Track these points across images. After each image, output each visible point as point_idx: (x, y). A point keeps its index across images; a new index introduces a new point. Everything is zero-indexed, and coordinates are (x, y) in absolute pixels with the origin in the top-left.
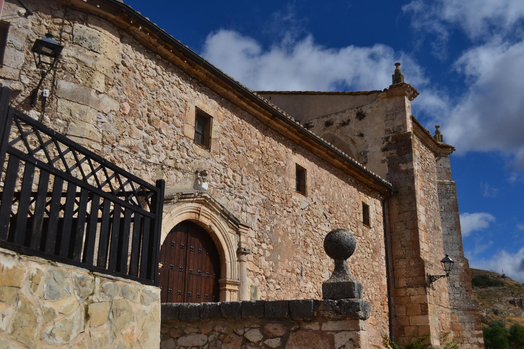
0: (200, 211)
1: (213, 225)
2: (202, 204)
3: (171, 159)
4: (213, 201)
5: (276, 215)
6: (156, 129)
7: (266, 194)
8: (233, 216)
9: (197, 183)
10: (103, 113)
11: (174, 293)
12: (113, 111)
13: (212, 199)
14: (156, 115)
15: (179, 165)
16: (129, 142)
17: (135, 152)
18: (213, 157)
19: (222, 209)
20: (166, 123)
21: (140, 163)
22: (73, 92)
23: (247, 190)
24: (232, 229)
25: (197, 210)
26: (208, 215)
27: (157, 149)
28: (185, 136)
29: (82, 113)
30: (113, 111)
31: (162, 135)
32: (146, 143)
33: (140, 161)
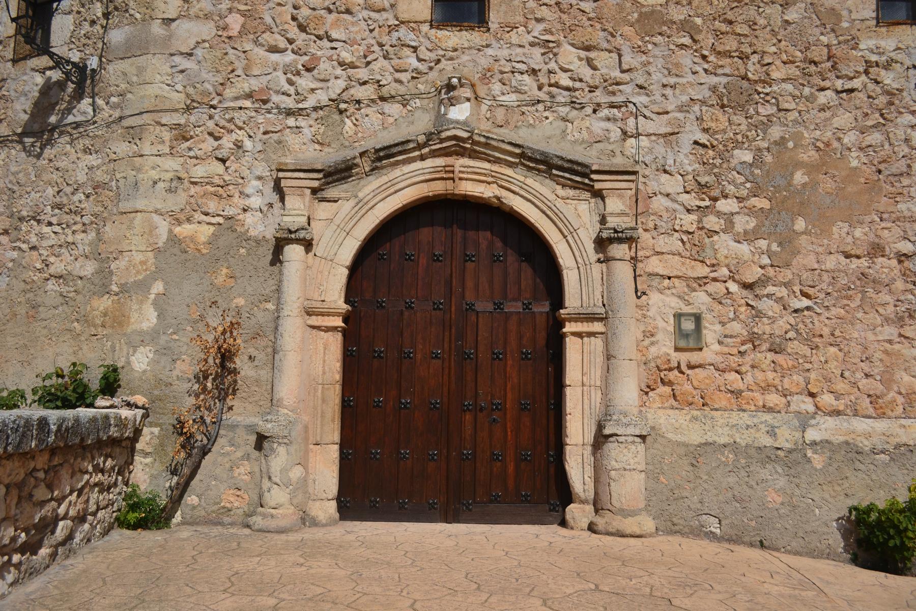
0: (453, 172)
1: (504, 193)
2: (457, 154)
3: (365, 83)
4: (483, 140)
5: (782, 114)
6: (320, 38)
7: (727, 70)
8: (562, 159)
9: (439, 110)
10: (182, 54)
11: (419, 356)
12: (204, 41)
13: (476, 138)
14: (314, 9)
15: (392, 89)
16: (245, 85)
17: (265, 102)
18: (498, 40)
19: (518, 151)
20: (346, 16)
21: (281, 117)
22: (128, 40)
23: (640, 81)
24: (575, 188)
25: (446, 172)
26: (485, 175)
27: (322, 77)
28: (402, 23)
29: (141, 70)
30: (204, 41)
31: (334, 44)
32: (292, 72)
33: (280, 113)
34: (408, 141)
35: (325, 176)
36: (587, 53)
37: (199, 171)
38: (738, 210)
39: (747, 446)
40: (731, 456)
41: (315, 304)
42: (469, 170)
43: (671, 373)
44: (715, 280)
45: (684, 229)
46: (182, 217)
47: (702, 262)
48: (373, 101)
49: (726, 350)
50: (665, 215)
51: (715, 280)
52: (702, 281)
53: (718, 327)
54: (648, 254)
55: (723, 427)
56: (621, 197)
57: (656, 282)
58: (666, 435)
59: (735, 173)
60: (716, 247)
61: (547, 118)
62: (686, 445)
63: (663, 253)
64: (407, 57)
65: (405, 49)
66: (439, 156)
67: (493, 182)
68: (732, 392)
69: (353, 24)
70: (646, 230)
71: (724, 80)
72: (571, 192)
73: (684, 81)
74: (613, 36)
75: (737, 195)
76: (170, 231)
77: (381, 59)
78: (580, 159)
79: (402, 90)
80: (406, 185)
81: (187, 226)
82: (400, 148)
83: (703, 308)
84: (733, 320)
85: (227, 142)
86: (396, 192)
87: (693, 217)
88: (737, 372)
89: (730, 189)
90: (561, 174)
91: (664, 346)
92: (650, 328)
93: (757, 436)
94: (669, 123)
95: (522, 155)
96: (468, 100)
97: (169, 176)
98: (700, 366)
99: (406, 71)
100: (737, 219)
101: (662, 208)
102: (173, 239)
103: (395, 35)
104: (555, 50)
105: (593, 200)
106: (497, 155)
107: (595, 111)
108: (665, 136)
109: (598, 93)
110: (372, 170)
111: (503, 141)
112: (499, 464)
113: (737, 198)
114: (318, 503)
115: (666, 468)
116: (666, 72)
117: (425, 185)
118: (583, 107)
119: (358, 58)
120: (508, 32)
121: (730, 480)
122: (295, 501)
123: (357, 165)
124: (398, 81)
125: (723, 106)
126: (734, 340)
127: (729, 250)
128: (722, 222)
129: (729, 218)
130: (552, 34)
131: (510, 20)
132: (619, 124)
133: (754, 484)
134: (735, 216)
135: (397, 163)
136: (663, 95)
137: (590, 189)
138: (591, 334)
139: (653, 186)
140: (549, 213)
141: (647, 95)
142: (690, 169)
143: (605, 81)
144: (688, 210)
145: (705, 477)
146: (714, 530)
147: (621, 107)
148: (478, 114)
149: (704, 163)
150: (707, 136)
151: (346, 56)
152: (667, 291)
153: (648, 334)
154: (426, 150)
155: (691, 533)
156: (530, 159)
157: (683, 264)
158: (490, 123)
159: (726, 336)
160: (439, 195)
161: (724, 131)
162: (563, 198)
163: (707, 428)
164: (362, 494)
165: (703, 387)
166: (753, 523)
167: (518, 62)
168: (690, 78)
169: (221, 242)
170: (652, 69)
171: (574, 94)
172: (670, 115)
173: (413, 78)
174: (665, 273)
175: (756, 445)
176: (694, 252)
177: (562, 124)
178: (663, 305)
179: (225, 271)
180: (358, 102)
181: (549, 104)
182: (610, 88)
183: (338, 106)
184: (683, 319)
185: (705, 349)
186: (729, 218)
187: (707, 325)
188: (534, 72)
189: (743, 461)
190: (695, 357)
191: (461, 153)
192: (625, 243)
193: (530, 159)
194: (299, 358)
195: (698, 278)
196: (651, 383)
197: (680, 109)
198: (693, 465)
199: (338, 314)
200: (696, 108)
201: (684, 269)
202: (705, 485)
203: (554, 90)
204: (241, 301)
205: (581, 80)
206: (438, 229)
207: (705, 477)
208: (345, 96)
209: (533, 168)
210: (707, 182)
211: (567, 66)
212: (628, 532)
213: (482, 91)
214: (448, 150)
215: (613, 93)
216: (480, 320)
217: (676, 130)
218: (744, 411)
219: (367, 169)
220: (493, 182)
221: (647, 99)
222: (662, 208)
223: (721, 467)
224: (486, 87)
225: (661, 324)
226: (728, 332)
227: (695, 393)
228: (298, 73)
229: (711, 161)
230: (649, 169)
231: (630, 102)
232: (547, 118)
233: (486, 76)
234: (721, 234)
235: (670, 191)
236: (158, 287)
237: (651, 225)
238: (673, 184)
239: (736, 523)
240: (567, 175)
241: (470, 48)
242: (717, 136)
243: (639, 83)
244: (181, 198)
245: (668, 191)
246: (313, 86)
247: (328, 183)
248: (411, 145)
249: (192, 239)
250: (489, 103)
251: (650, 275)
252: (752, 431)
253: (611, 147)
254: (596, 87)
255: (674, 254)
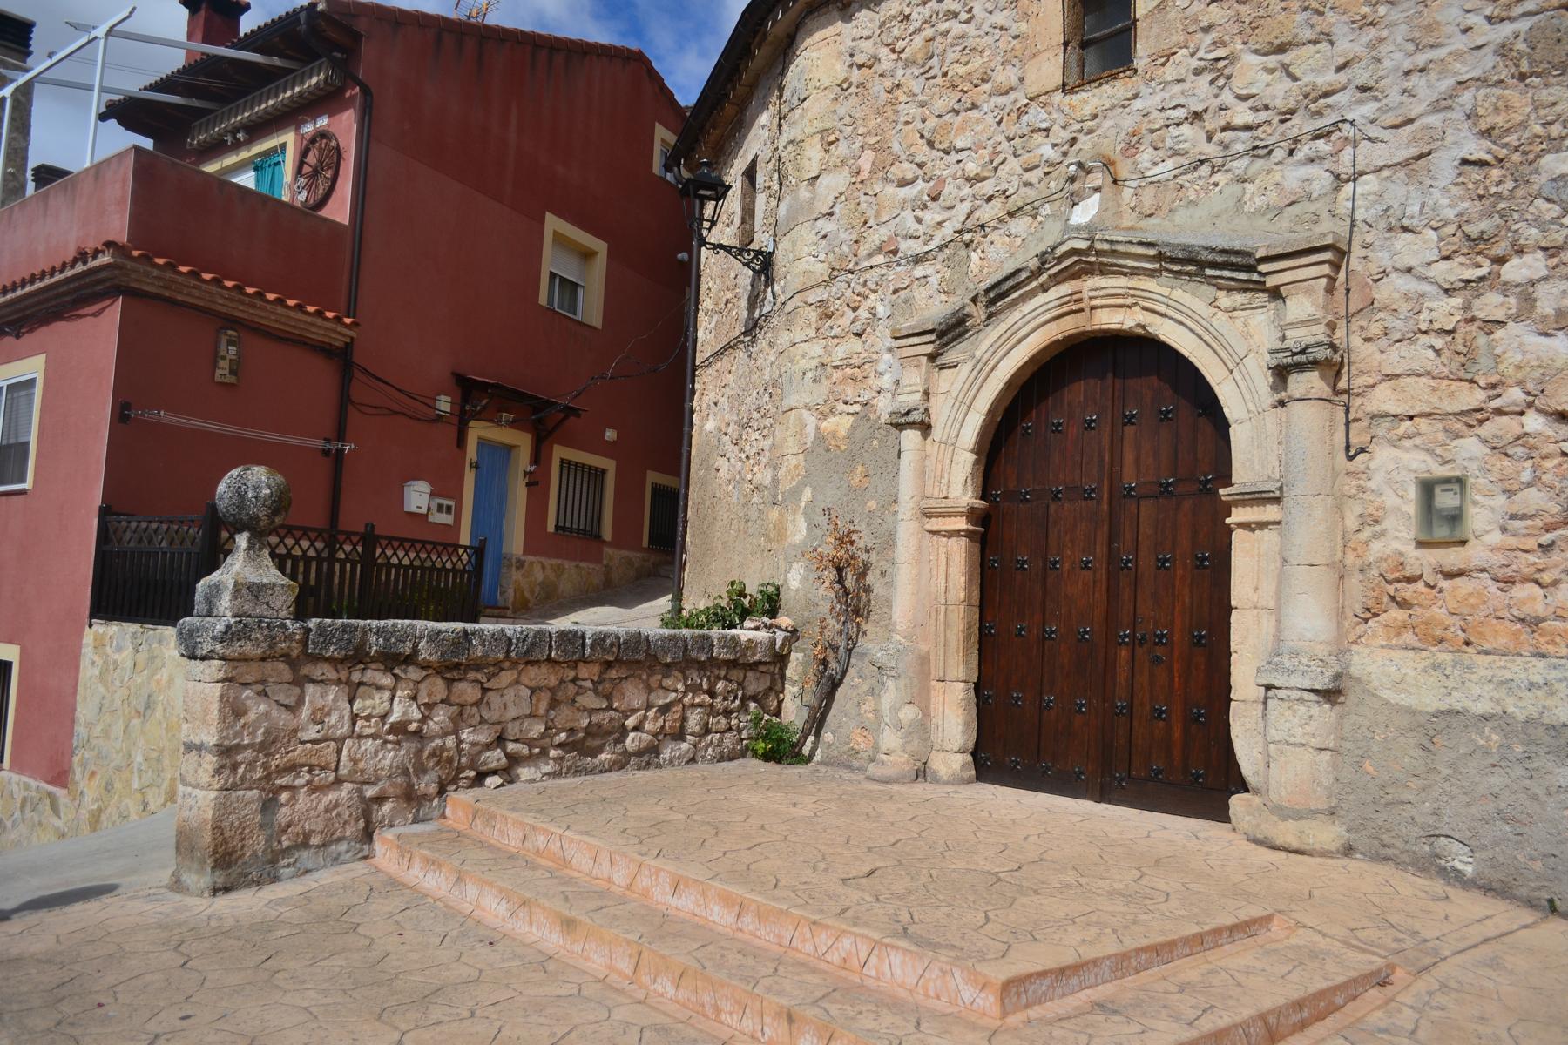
3: (990, 199)
4: (1106, 247)
8: (1213, 250)
13: (1098, 246)
17: (895, 252)
19: (1152, 252)
24: (1245, 290)
34: (1018, 271)
35: (940, 337)
36: (1279, 57)
37: (839, 353)
38: (1545, 272)
39: (1528, 721)
40: (1495, 737)
41: (932, 503)
42: (1102, 293)
43: (1412, 587)
44: (1499, 412)
45: (1437, 326)
46: (826, 410)
47: (1472, 381)
48: (1001, 220)
49: (1513, 542)
50: (1404, 308)
51: (1499, 412)
52: (1476, 417)
53: (1500, 500)
54: (1371, 381)
55: (1478, 688)
56: (1307, 292)
57: (1382, 428)
58: (1379, 693)
59: (1540, 202)
60: (1498, 351)
61: (1216, 185)
62: (1412, 712)
63: (1398, 376)
64: (1039, 146)
65: (1035, 136)
66: (1064, 281)
67: (1136, 304)
68: (1523, 620)
69: (978, 121)
70: (1367, 340)
71: (1523, 25)
72: (1239, 298)
73: (1441, 53)
74: (1321, 14)
75: (1543, 244)
76: (818, 428)
77: (1011, 158)
78: (1237, 245)
79: (1031, 194)
80: (1028, 331)
81: (832, 420)
82: (1011, 283)
83: (1473, 467)
84: (1529, 485)
85: (863, 313)
86: (1020, 341)
87: (1457, 301)
88: (1537, 582)
89: (1532, 234)
90: (1218, 273)
91: (1398, 536)
92: (1370, 510)
93: (1549, 702)
94: (1414, 139)
95: (1160, 257)
96: (1097, 190)
97: (815, 362)
98: (1460, 573)
99: (1037, 167)
100: (1541, 291)
101: (1397, 295)
102: (820, 438)
103: (1025, 118)
104: (1226, 71)
105: (1272, 305)
106: (1130, 263)
107: (1291, 152)
108: (1406, 163)
109: (1296, 120)
110: (989, 317)
111: (1131, 243)
112: (1162, 724)
113: (1545, 249)
114: (942, 755)
115: (1375, 748)
116: (1411, 47)
117: (1053, 325)
118: (1270, 152)
119: (983, 166)
120: (1163, 65)
121: (1494, 780)
122: (909, 748)
123: (969, 316)
124: (1028, 184)
125: (1522, 77)
126: (1529, 522)
127: (1524, 352)
128: (1512, 300)
129: (1526, 293)
130: (1224, 44)
131: (1164, 46)
132: (1327, 164)
133: (1540, 792)
134: (1538, 286)
135: (1015, 303)
136: (1405, 91)
137: (1259, 287)
138: (1262, 525)
139: (1381, 258)
140: (1207, 337)
141: (1376, 99)
142: (1450, 214)
143: (1306, 96)
144: (1446, 291)
145: (1446, 772)
146: (1459, 866)
147: (1329, 134)
148: (1119, 206)
149: (1481, 197)
150: (1487, 144)
151: (972, 168)
152: (1407, 443)
153: (1369, 520)
154: (1044, 277)
155: (1412, 864)
156: (1173, 260)
157: (1434, 390)
158: (1135, 214)
159: (1513, 517)
160: (1070, 337)
161: (1524, 125)
162: (1227, 311)
163: (1450, 684)
164: (1004, 750)
165: (1465, 611)
166: (1538, 866)
167: (1174, 108)
168: (1460, 43)
169: (858, 435)
170: (1383, 50)
171: (1255, 133)
172: (1416, 124)
173: (1047, 174)
174: (1399, 411)
175: (1546, 720)
176: (1455, 366)
177: (1237, 188)
178: (1396, 469)
179: (860, 468)
180: (982, 226)
181: (1219, 161)
182: (1313, 107)
183: (970, 235)
184: (1438, 490)
185: (1472, 542)
186: (1526, 293)
187: (1478, 498)
188: (1197, 116)
189: (1520, 749)
190: (1452, 558)
191: (1089, 270)
192: (1311, 369)
193: (1173, 260)
194: (914, 572)
195: (1462, 413)
196: (1370, 604)
197: (1436, 107)
198: (1424, 748)
199: (960, 514)
200: (1466, 98)
201: (1434, 400)
202: (1447, 786)
203: (1229, 135)
204: (872, 505)
205: (1267, 108)
206: (1092, 381)
207: (1446, 772)
208: (969, 225)
209: (1180, 273)
210: (1482, 232)
211: (1244, 92)
212: (1279, 842)
213: (1123, 171)
214: (1071, 271)
215: (1319, 113)
216: (1142, 509)
217: (1425, 150)
218: (1543, 656)
219: (983, 317)
220: (1136, 304)
221: (1376, 105)
222: (1397, 295)
223: (1477, 756)
224: (1130, 161)
225: (1390, 500)
226: (1515, 509)
227: (1449, 620)
228: (925, 207)
229: (1493, 190)
230: (1374, 231)
231: (1344, 121)
232: (1216, 185)
233: (1132, 145)
234: (1511, 324)
235: (1412, 262)
236: (807, 494)
237: (1375, 329)
238: (1417, 249)
239: (1501, 859)
240: (1226, 273)
241: (1113, 107)
242: (1507, 140)
243: (1359, 82)
244: (823, 389)
245: (1409, 268)
246: (939, 219)
247: (946, 345)
248: (1024, 275)
249: (834, 434)
250: (1134, 184)
251: (1374, 417)
252: (1539, 693)
253: (1312, 208)
254: (1293, 112)
255: (1420, 375)
